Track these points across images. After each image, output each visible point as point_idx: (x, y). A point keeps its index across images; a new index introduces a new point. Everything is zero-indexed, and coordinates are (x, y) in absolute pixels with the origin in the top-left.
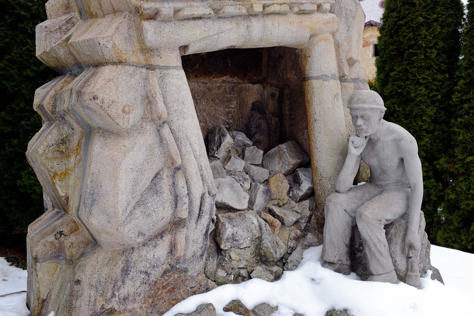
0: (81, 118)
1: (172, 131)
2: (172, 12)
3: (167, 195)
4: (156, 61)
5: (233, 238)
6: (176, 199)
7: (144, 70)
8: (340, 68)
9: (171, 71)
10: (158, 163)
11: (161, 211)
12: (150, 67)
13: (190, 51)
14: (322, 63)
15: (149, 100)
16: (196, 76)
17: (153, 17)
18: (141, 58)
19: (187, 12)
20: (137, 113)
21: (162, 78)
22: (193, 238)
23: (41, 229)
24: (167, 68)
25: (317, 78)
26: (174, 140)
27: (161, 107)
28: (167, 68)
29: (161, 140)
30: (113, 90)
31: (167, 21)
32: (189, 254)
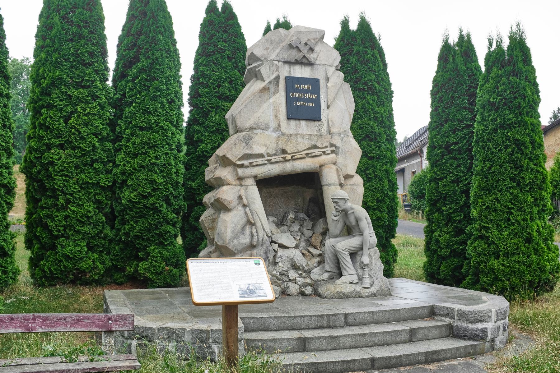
0: (181, 329)
1: (250, 210)
2: (248, 164)
5: (281, 257)
6: (252, 235)
7: (239, 187)
8: (339, 180)
9: (249, 187)
10: (244, 220)
11: (245, 240)
12: (241, 185)
13: (258, 179)
14: (330, 177)
15: (240, 198)
16: (277, 187)
17: (242, 166)
18: (238, 182)
19: (255, 164)
20: (235, 202)
21: (246, 189)
23: (248, 101)
25: (326, 185)
26: (348, 359)
27: (245, 201)
28: (247, 185)
29: (246, 213)
30: (227, 194)
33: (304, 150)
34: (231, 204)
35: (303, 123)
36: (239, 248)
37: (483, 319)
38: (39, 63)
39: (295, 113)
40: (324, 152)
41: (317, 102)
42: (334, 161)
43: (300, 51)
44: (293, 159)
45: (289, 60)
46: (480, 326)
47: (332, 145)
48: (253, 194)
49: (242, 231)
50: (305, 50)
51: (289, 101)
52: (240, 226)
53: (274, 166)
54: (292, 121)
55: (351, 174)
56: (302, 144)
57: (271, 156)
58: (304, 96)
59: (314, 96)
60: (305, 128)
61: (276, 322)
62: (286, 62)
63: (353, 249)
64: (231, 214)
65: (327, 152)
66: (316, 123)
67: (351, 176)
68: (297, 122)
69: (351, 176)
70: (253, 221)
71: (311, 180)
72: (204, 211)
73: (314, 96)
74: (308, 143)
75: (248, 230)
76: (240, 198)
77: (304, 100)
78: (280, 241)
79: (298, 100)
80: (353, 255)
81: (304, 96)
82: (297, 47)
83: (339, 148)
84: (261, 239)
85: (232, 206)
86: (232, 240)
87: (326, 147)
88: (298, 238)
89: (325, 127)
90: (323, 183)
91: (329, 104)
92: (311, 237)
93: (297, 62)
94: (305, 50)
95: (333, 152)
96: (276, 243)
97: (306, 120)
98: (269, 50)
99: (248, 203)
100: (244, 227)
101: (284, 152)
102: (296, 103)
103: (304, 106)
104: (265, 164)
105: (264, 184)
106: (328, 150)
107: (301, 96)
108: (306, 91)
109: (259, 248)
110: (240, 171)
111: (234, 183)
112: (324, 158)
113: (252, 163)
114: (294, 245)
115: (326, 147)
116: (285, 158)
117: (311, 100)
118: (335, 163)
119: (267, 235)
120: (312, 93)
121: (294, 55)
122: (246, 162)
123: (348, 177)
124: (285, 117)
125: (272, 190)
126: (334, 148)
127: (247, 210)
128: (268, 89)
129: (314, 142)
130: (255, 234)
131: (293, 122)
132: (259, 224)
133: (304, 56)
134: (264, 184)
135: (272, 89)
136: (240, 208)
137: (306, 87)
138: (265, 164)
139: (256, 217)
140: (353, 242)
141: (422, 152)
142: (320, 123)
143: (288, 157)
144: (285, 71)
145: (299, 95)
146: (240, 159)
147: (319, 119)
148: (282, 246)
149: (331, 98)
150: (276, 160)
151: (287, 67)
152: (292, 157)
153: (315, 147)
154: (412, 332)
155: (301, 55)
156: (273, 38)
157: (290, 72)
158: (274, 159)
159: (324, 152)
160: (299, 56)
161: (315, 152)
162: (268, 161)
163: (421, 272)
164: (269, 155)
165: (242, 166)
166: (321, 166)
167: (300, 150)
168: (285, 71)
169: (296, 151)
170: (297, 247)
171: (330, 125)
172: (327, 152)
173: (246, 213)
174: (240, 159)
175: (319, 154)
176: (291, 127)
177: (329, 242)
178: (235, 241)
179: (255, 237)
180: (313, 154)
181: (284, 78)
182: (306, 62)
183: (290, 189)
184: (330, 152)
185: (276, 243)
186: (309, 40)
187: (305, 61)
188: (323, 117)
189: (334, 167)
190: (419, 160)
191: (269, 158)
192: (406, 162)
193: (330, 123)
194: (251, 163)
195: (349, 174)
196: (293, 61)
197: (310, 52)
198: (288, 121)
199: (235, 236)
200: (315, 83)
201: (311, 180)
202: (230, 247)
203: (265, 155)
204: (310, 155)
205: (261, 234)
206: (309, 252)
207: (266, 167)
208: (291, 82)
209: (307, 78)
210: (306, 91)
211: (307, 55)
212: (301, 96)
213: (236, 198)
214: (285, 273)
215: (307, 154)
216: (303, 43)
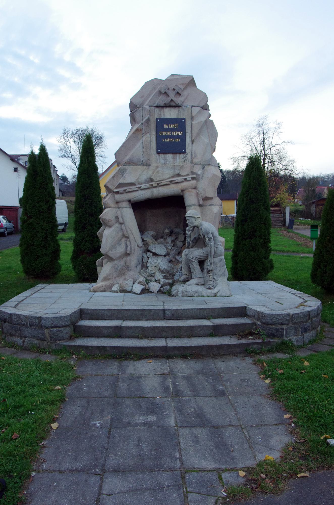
3: (123, 245)
10: (120, 234)
11: (121, 250)
12: (119, 208)
15: (117, 217)
17: (118, 193)
18: (116, 206)
19: (127, 191)
24: (123, 208)
31: (122, 193)
33: (169, 178)
34: (110, 223)
39: (164, 148)
40: (185, 179)
41: (183, 138)
42: (194, 186)
43: (169, 96)
44: (159, 185)
47: (193, 173)
48: (129, 215)
50: (172, 95)
51: (159, 138)
53: (143, 192)
54: (161, 155)
55: (210, 196)
58: (171, 133)
59: (180, 133)
62: (157, 107)
63: (202, 258)
65: (188, 179)
67: (211, 198)
69: (211, 198)
71: (176, 203)
73: (180, 133)
75: (124, 240)
76: (117, 217)
78: (153, 251)
80: (201, 263)
81: (171, 133)
82: (165, 93)
83: (199, 175)
85: (111, 223)
86: (110, 250)
87: (188, 175)
89: (189, 158)
90: (186, 205)
91: (193, 138)
92: (182, 247)
94: (172, 95)
95: (193, 178)
96: (150, 252)
97: (173, 153)
98: (144, 98)
99: (124, 221)
101: (152, 180)
102: (165, 140)
103: (171, 143)
104: (136, 191)
105: (138, 207)
106: (188, 178)
107: (169, 133)
108: (173, 130)
110: (117, 197)
112: (185, 184)
113: (125, 190)
114: (164, 254)
115: (188, 175)
116: (152, 185)
117: (178, 137)
118: (195, 188)
119: (138, 246)
120: (178, 131)
121: (162, 100)
122: (121, 190)
123: (206, 199)
126: (194, 176)
128: (141, 130)
129: (177, 172)
131: (162, 156)
132: (131, 237)
133: (172, 100)
134: (138, 207)
137: (173, 126)
138: (136, 191)
142: (185, 155)
143: (154, 184)
144: (157, 113)
145: (167, 133)
146: (117, 187)
147: (184, 153)
148: (155, 254)
149: (194, 134)
150: (145, 187)
151: (157, 110)
152: (158, 184)
153: (179, 175)
155: (169, 99)
157: (160, 114)
158: (143, 186)
159: (185, 179)
160: (167, 100)
161: (178, 179)
162: (139, 188)
163: (306, 275)
164: (140, 183)
165: (118, 193)
166: (182, 191)
168: (157, 113)
169: (161, 179)
170: (168, 254)
171: (193, 157)
172: (188, 179)
173: (122, 229)
174: (117, 187)
175: (181, 181)
176: (158, 160)
177: (185, 252)
179: (129, 248)
180: (175, 182)
182: (174, 104)
184: (190, 179)
185: (150, 252)
186: (176, 85)
187: (173, 104)
188: (187, 151)
189: (194, 191)
191: (139, 186)
193: (193, 154)
194: (125, 190)
195: (208, 196)
196: (162, 105)
198: (157, 155)
199: (114, 247)
201: (176, 203)
203: (137, 184)
204: (173, 182)
206: (176, 259)
207: (136, 193)
208: (161, 124)
209: (174, 119)
211: (174, 99)
212: (169, 133)
213: (114, 218)
214: (153, 275)
215: (171, 181)
216: (171, 88)
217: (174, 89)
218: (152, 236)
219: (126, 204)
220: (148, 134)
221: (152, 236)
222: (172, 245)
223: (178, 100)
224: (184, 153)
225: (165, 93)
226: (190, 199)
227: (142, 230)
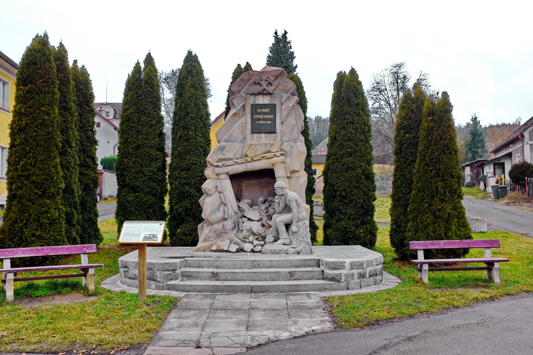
4: (220, 177)
6: (225, 212)
10: (219, 202)
11: (219, 215)
12: (218, 179)
15: (217, 187)
17: (218, 166)
18: (216, 177)
19: (226, 165)
20: (214, 190)
22: (229, 224)
27: (220, 189)
31: (221, 167)
32: (228, 228)
35: (263, 135)
36: (216, 220)
37: (338, 267)
38: (126, 102)
40: (275, 155)
41: (274, 120)
45: (253, 92)
46: (336, 272)
47: (282, 150)
48: (227, 184)
49: (218, 210)
51: (253, 120)
52: (216, 206)
53: (239, 166)
55: (297, 169)
56: (260, 150)
57: (238, 159)
59: (271, 117)
60: (264, 139)
61: (207, 263)
64: (211, 198)
66: (273, 135)
68: (259, 135)
70: (225, 203)
71: (267, 175)
72: (201, 196)
73: (271, 117)
74: (264, 149)
75: (222, 206)
77: (264, 119)
78: (248, 216)
79: (259, 120)
82: (259, 83)
84: (230, 214)
86: (210, 215)
87: (277, 152)
88: (263, 214)
89: (279, 137)
90: (276, 177)
93: (259, 94)
95: (282, 155)
96: (246, 217)
100: (220, 206)
101: (246, 156)
103: (264, 124)
105: (235, 178)
106: (278, 154)
107: (262, 117)
108: (265, 113)
109: (229, 220)
110: (216, 169)
111: (213, 177)
112: (276, 159)
115: (277, 152)
118: (284, 163)
120: (270, 115)
122: (220, 164)
124: (250, 132)
125: (250, 181)
126: (283, 152)
127: (222, 195)
129: (268, 149)
130: (226, 210)
131: (255, 135)
132: (229, 204)
134: (235, 178)
135: (241, 114)
136: (217, 194)
139: (227, 200)
140: (286, 217)
141: (523, 136)
142: (275, 135)
147: (275, 132)
151: (252, 97)
152: (252, 159)
153: (269, 152)
154: (291, 274)
155: (262, 88)
156: (244, 78)
158: (239, 161)
159: (275, 155)
161: (269, 155)
162: (236, 162)
165: (218, 166)
167: (257, 154)
173: (220, 197)
174: (217, 162)
175: (271, 156)
178: (213, 216)
179: (226, 213)
181: (250, 105)
182: (266, 92)
183: (264, 180)
185: (246, 217)
187: (265, 92)
188: (278, 131)
189: (283, 165)
190: (521, 145)
192: (512, 147)
194: (223, 164)
197: (270, 86)
199: (213, 212)
200: (272, 108)
202: (210, 219)
203: (234, 159)
205: (230, 211)
208: (255, 108)
210: (265, 113)
211: (266, 88)
212: (262, 117)
215: (263, 157)
217: (266, 80)
218: (248, 203)
219: (224, 176)
220: (244, 117)
221: (248, 203)
222: (265, 211)
223: (270, 89)
224: (275, 132)
225: (259, 83)
226: (279, 172)
227: (239, 198)
